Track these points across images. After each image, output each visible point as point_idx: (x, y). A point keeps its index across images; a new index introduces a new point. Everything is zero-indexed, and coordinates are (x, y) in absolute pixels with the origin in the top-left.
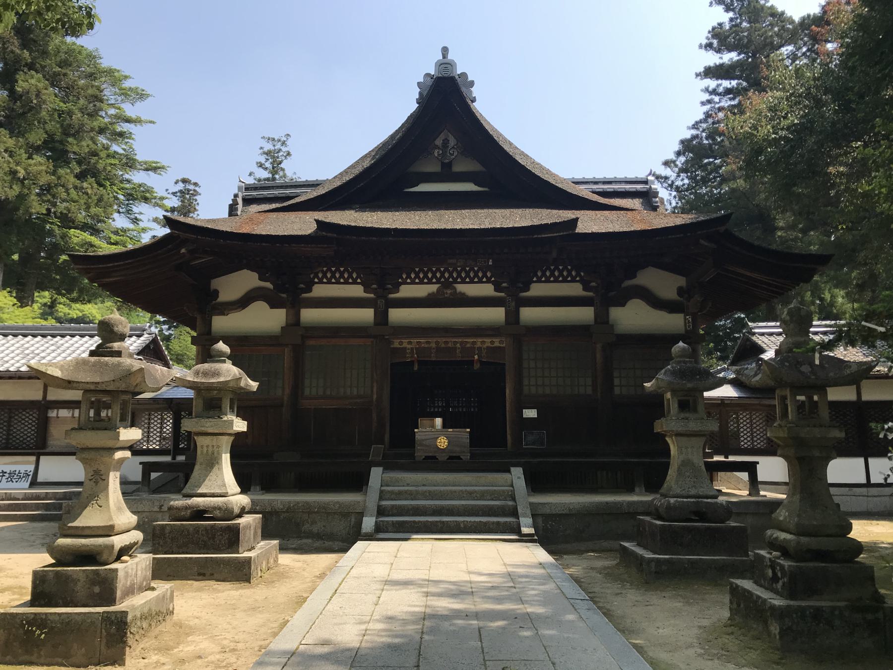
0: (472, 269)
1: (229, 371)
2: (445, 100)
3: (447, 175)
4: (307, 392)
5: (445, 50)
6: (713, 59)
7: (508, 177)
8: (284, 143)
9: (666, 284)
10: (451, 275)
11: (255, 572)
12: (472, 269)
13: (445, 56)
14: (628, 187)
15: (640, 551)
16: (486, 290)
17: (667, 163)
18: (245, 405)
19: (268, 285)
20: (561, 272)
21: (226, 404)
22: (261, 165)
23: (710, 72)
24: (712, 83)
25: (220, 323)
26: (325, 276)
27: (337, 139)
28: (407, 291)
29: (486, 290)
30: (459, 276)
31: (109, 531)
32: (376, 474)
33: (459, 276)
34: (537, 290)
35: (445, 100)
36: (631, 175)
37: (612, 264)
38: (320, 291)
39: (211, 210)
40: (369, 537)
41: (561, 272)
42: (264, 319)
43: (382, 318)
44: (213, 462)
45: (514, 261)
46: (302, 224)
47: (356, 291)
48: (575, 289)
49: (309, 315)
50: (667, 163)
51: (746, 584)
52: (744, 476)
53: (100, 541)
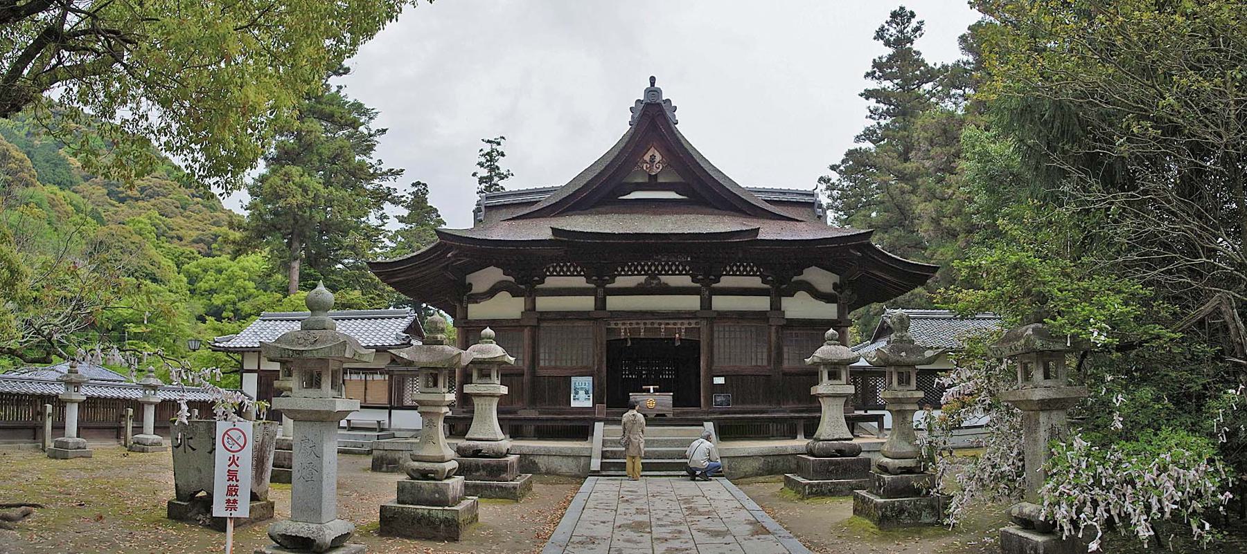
0: (674, 263)
1: (496, 351)
2: (653, 118)
3: (652, 184)
4: (542, 363)
5: (653, 80)
6: (873, 85)
7: (703, 187)
8: (499, 144)
9: (823, 279)
10: (656, 269)
11: (464, 535)
12: (674, 263)
13: (653, 84)
14: (799, 198)
15: (800, 479)
16: (686, 281)
17: (833, 168)
18: (508, 376)
19: (510, 279)
20: (745, 268)
21: (494, 374)
22: (481, 164)
23: (868, 94)
24: (872, 103)
25: (476, 311)
26: (555, 270)
27: (558, 147)
28: (621, 282)
29: (686, 281)
30: (663, 269)
31: (442, 460)
32: (599, 427)
33: (663, 269)
34: (726, 281)
35: (653, 118)
36: (801, 188)
37: (783, 266)
38: (551, 282)
39: (458, 214)
40: (595, 473)
41: (745, 268)
42: (509, 307)
43: (601, 304)
44: (484, 420)
45: (707, 259)
46: (540, 231)
47: (580, 282)
48: (756, 282)
49: (543, 303)
50: (833, 168)
51: (863, 493)
52: (875, 424)
53: (437, 465)
